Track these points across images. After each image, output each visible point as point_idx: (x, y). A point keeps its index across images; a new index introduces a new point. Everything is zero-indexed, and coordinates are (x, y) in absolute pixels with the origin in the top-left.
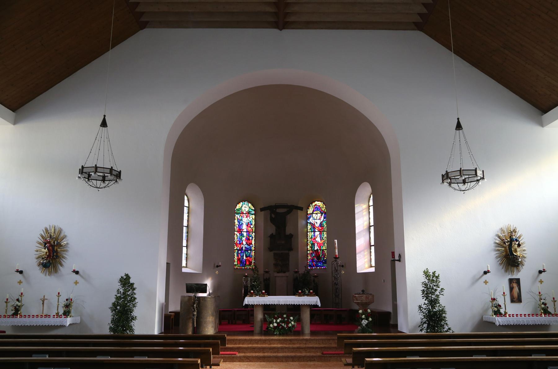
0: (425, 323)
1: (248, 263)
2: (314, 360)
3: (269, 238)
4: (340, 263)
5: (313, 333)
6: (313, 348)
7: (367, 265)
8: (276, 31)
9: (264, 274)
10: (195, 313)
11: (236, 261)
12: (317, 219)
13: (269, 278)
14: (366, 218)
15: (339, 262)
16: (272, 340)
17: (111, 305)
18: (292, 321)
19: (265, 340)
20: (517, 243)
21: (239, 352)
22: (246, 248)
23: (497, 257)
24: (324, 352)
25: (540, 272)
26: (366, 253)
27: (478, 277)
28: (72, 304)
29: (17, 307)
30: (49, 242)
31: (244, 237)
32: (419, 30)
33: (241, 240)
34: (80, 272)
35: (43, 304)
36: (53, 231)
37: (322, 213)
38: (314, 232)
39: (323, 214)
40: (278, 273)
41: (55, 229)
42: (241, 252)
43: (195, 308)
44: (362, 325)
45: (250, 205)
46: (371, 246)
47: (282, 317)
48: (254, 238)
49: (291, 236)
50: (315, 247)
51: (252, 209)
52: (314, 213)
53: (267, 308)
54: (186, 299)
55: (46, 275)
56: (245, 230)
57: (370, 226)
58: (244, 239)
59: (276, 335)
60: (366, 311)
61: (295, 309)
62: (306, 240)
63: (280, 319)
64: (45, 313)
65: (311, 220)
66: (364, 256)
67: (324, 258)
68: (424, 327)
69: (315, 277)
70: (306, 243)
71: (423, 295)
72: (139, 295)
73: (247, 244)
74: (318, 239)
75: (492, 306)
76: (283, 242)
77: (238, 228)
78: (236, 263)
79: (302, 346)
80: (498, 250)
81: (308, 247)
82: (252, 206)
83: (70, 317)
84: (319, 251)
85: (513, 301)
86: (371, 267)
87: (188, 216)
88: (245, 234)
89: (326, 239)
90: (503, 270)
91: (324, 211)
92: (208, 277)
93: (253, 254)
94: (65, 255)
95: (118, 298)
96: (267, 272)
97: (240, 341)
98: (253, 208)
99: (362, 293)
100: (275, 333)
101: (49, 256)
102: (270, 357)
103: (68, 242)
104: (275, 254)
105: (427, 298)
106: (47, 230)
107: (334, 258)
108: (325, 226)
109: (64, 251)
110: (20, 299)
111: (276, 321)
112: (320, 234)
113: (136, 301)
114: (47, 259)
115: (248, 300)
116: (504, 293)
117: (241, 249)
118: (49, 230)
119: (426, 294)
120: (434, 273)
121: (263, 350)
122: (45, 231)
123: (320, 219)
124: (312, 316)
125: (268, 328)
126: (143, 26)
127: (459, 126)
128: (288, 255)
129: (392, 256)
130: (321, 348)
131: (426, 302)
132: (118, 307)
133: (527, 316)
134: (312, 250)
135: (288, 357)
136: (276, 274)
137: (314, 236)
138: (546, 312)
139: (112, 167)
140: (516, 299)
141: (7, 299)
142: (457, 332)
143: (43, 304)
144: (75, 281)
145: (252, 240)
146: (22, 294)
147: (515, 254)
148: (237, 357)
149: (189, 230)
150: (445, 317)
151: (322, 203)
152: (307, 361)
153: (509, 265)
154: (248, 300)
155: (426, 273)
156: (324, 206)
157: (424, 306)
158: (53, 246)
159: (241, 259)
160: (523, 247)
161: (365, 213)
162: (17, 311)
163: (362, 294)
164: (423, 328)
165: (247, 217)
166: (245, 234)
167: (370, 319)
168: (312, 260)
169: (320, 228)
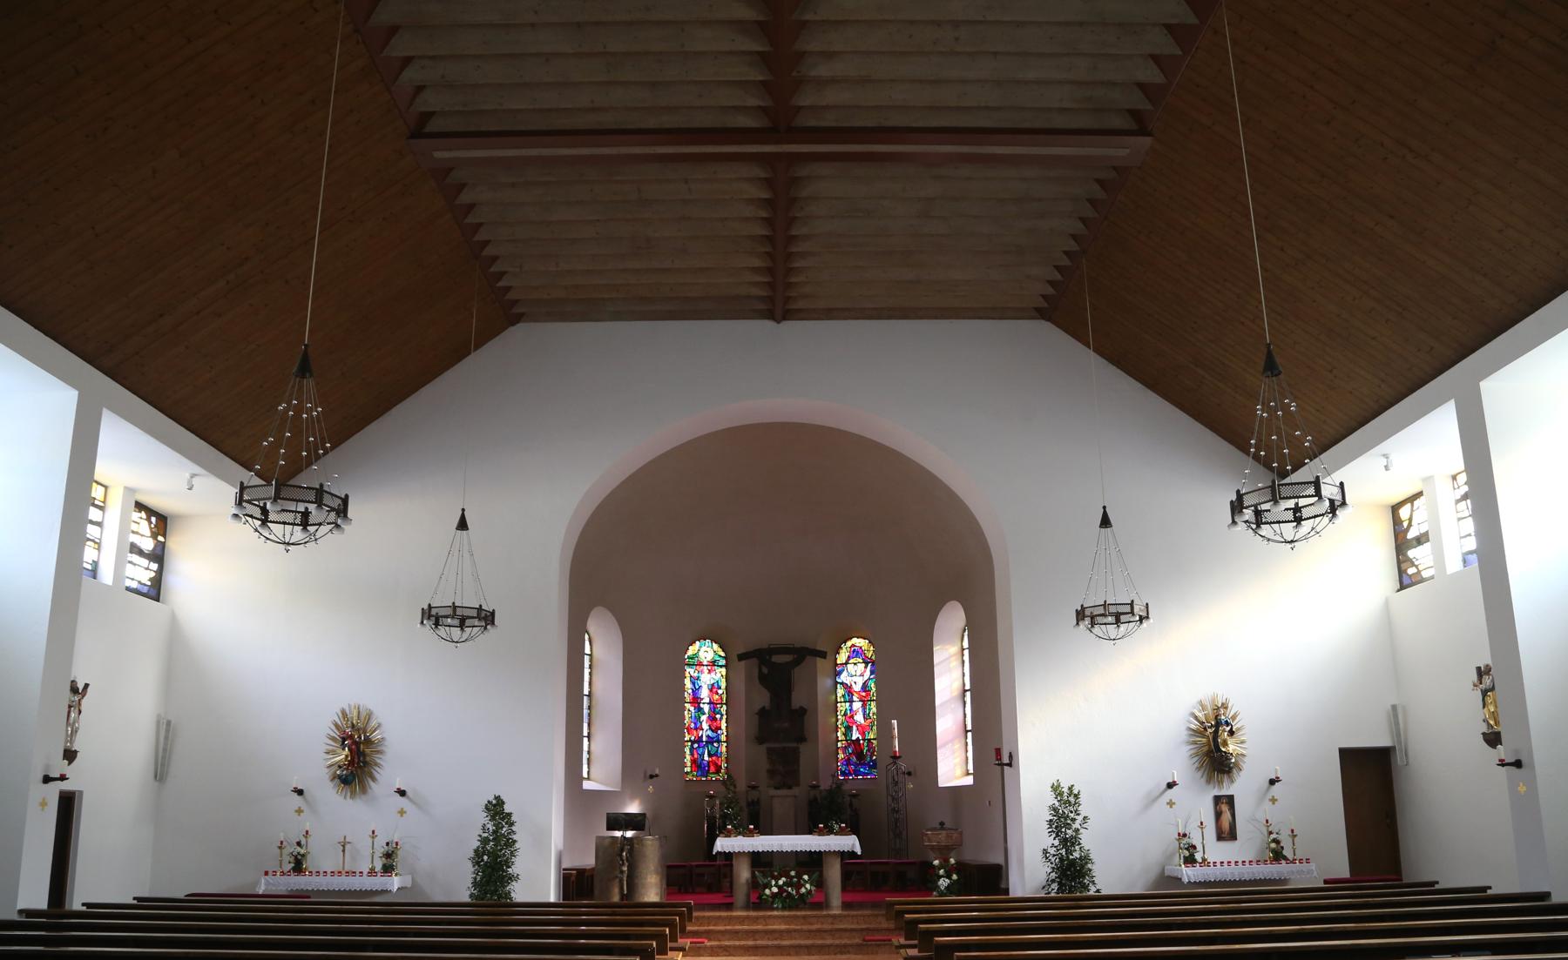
0: (1053, 881)
1: (712, 769)
2: (849, 952)
3: (757, 716)
4: (903, 768)
5: (846, 905)
6: (845, 930)
7: (959, 771)
8: (769, 324)
9: (747, 792)
10: (625, 869)
11: (689, 764)
12: (856, 675)
13: (758, 800)
14: (957, 674)
15: (903, 765)
16: (770, 917)
17: (472, 854)
18: (806, 882)
19: (757, 918)
20: (1228, 728)
21: (710, 940)
22: (708, 736)
23: (1192, 756)
24: (867, 938)
25: (1272, 782)
26: (958, 746)
27: (1158, 794)
28: (399, 852)
29: (299, 857)
30: (351, 737)
31: (704, 714)
32: (1043, 318)
33: (697, 720)
34: (409, 793)
35: (344, 851)
36: (355, 714)
37: (866, 664)
38: (851, 701)
39: (870, 665)
40: (776, 788)
41: (359, 712)
42: (699, 747)
43: (624, 858)
44: (939, 887)
45: (715, 646)
46: (967, 731)
47: (788, 876)
48: (725, 717)
49: (802, 712)
50: (854, 735)
51: (720, 656)
52: (850, 662)
53: (759, 860)
54: (607, 842)
55: (345, 798)
56: (707, 700)
57: (965, 691)
58: (704, 718)
59: (777, 909)
60: (946, 860)
61: (812, 861)
62: (834, 720)
63: (784, 879)
64: (347, 869)
65: (844, 678)
66: (954, 752)
67: (871, 757)
68: (1053, 889)
69: (854, 796)
70: (834, 725)
71: (1050, 830)
72: (521, 836)
73: (710, 729)
74: (859, 718)
75: (1180, 848)
76: (786, 725)
77: (691, 697)
78: (688, 769)
79: (826, 927)
80: (1195, 743)
81: (839, 734)
82: (720, 649)
83: (396, 875)
84: (861, 742)
85: (1220, 837)
86: (968, 774)
87: (590, 674)
88: (706, 708)
89: (875, 717)
90: (1204, 780)
91: (870, 659)
92: (633, 798)
93: (724, 749)
94: (378, 761)
95: (484, 841)
96: (754, 788)
97: (710, 920)
98: (723, 654)
99: (939, 827)
100: (775, 906)
101: (351, 763)
102: (767, 947)
103: (384, 736)
104: (770, 751)
105: (1057, 835)
106: (344, 713)
107: (892, 757)
108: (874, 689)
109: (378, 752)
110: (303, 842)
111: (777, 883)
112: (864, 706)
113: (517, 845)
114: (347, 769)
115: (722, 844)
116: (1202, 823)
117: (699, 740)
118: (348, 712)
119: (1056, 827)
120: (1070, 788)
121: (753, 934)
122: (340, 715)
123: (862, 675)
124: (846, 876)
125: (760, 897)
126: (515, 320)
127: (1105, 522)
128: (796, 752)
129: (997, 756)
130: (862, 930)
131: (1056, 842)
132: (485, 858)
133: (1247, 863)
134: (846, 740)
135: (800, 946)
136: (773, 792)
137: (851, 710)
138: (1278, 856)
139: (481, 606)
140: (1227, 834)
141: (282, 843)
142: (1104, 892)
143: (344, 851)
144: (400, 810)
145: (721, 720)
146: (307, 832)
147: (1223, 749)
148: (706, 947)
149: (594, 703)
150: (1090, 870)
151: (867, 641)
152: (835, 954)
153: (1214, 771)
154: (722, 844)
155: (1056, 789)
156: (872, 648)
157: (1052, 851)
158: (357, 744)
159: (699, 761)
160: (1239, 736)
161: (955, 663)
162: (298, 866)
163: (940, 829)
164: (1050, 890)
165: (710, 672)
166: (706, 708)
167: (955, 877)
168: (848, 762)
169: (864, 694)
